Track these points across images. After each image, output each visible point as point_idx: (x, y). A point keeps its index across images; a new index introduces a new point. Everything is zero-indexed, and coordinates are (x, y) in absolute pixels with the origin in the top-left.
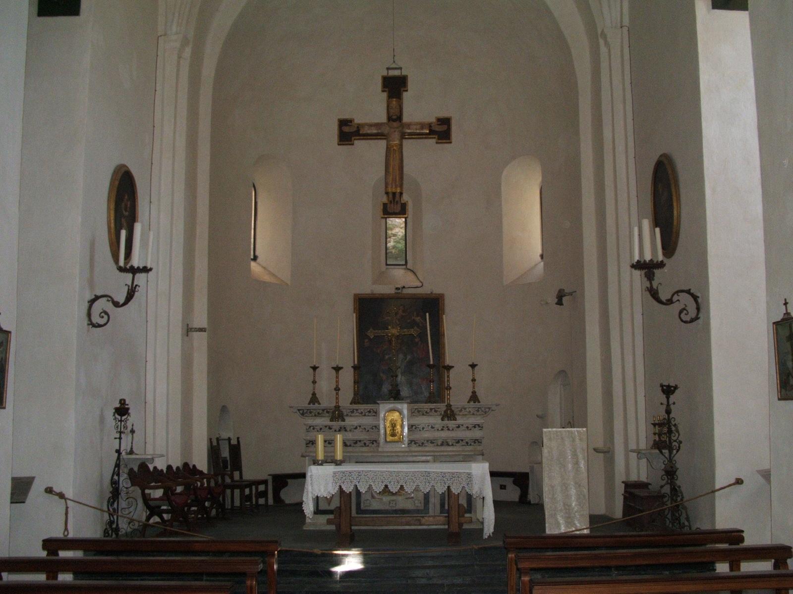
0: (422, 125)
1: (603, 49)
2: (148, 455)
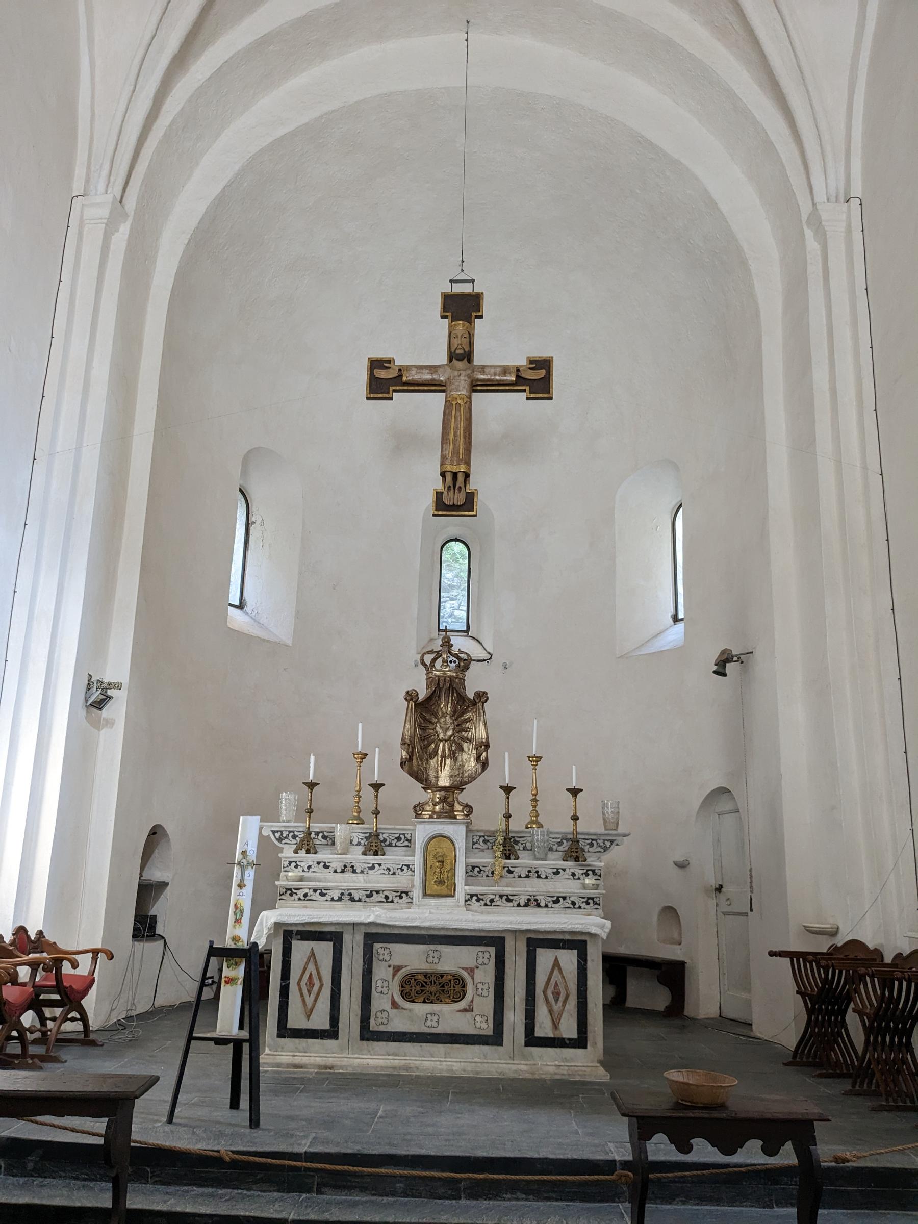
0: (505, 370)
1: (812, 244)
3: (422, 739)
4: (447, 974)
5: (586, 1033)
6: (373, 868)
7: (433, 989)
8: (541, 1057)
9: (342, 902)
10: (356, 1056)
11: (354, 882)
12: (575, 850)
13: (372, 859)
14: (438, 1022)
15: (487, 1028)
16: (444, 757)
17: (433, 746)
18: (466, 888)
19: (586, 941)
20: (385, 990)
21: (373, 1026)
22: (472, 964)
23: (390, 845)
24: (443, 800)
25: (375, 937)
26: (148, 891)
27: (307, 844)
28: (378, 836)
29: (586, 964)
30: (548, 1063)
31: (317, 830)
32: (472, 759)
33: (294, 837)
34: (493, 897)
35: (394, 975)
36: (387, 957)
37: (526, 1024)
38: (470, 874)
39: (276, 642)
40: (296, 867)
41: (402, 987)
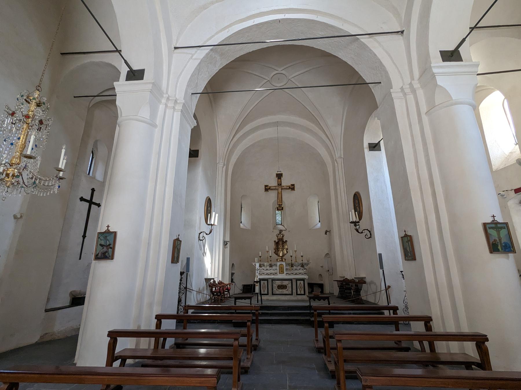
0: (287, 186)
1: (336, 164)
2: (345, 382)
12: (302, 266)
25: (273, 280)
26: (232, 274)
30: (300, 297)
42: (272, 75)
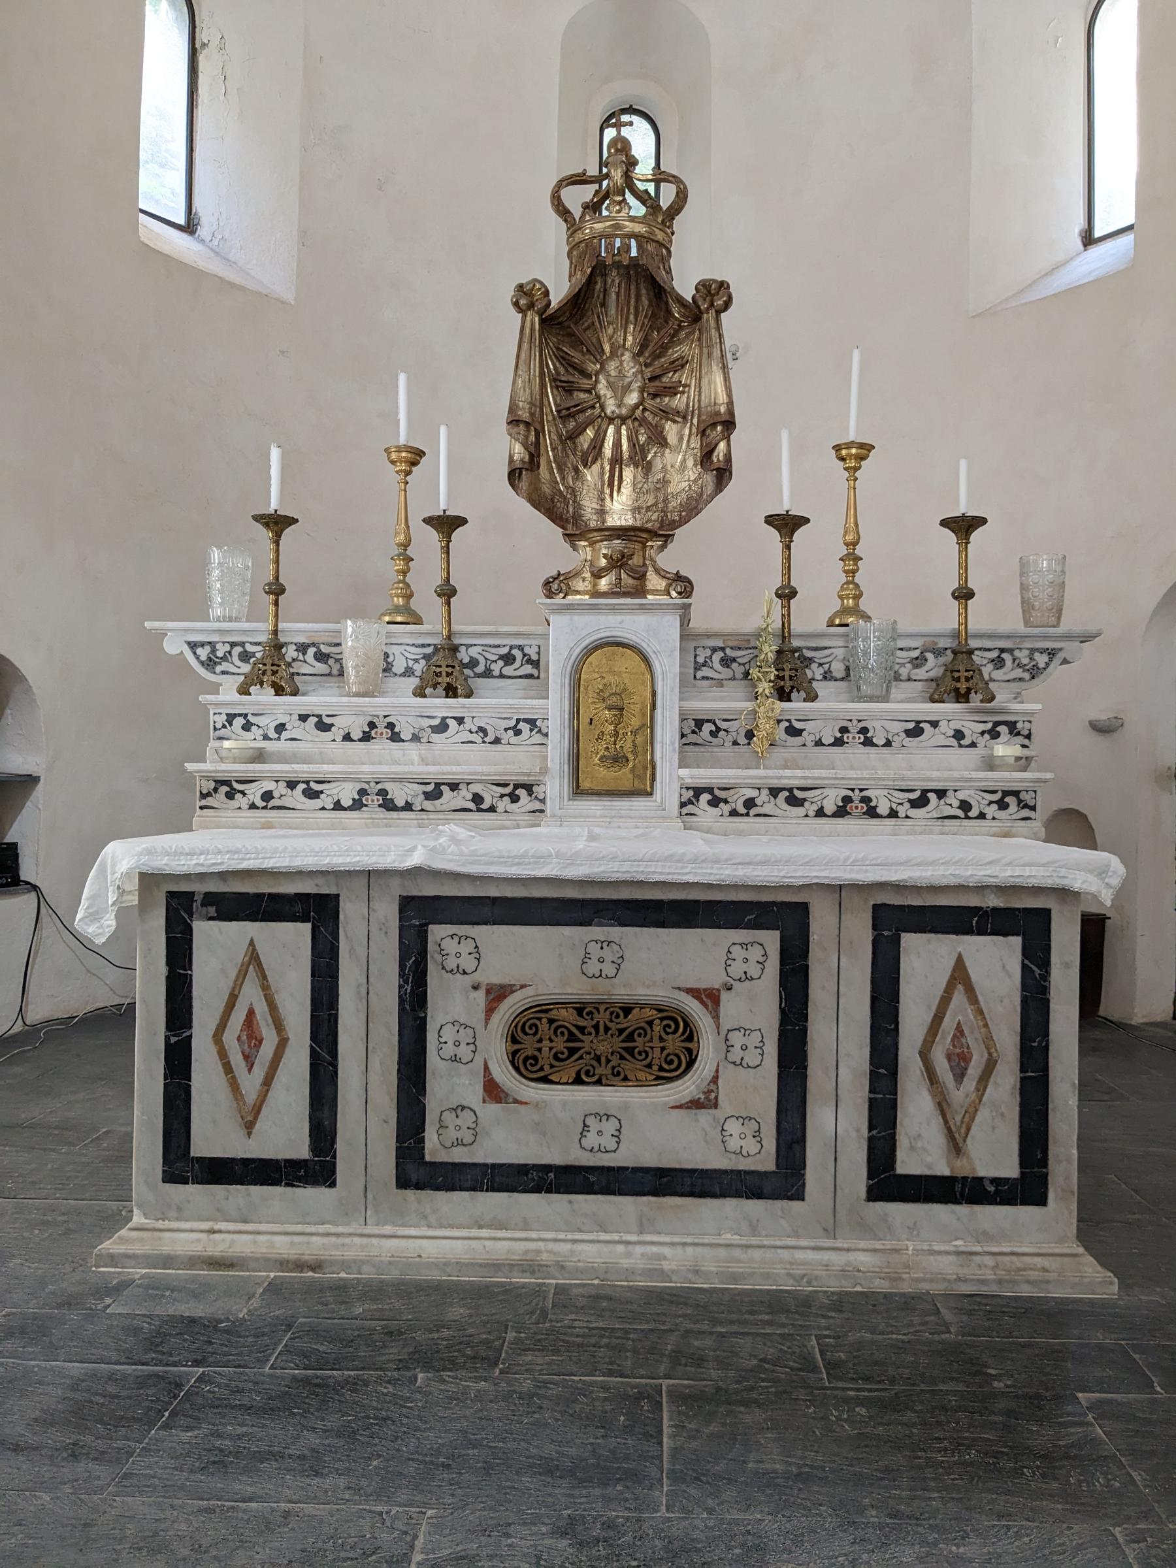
3: (565, 414)
4: (642, 1006)
5: (1044, 1162)
6: (442, 727)
7: (603, 1048)
8: (913, 1229)
9: (364, 813)
10: (388, 1229)
11: (396, 762)
12: (959, 674)
13: (440, 706)
14: (617, 1136)
15: (761, 1155)
16: (617, 460)
17: (590, 433)
18: (684, 772)
19: (1046, 913)
20: (464, 1052)
21: (434, 1147)
22: (712, 978)
23: (487, 674)
24: (618, 563)
25: (428, 910)
27: (274, 669)
28: (455, 649)
29: (1046, 976)
31: (302, 639)
32: (690, 463)
33: (245, 657)
34: (752, 793)
35: (490, 1011)
36: (468, 963)
37: (871, 1140)
38: (692, 738)
39: (259, 293)
40: (247, 727)
41: (514, 1040)
42: (683, 1057)
